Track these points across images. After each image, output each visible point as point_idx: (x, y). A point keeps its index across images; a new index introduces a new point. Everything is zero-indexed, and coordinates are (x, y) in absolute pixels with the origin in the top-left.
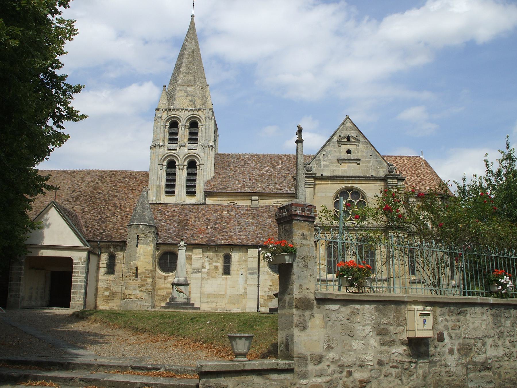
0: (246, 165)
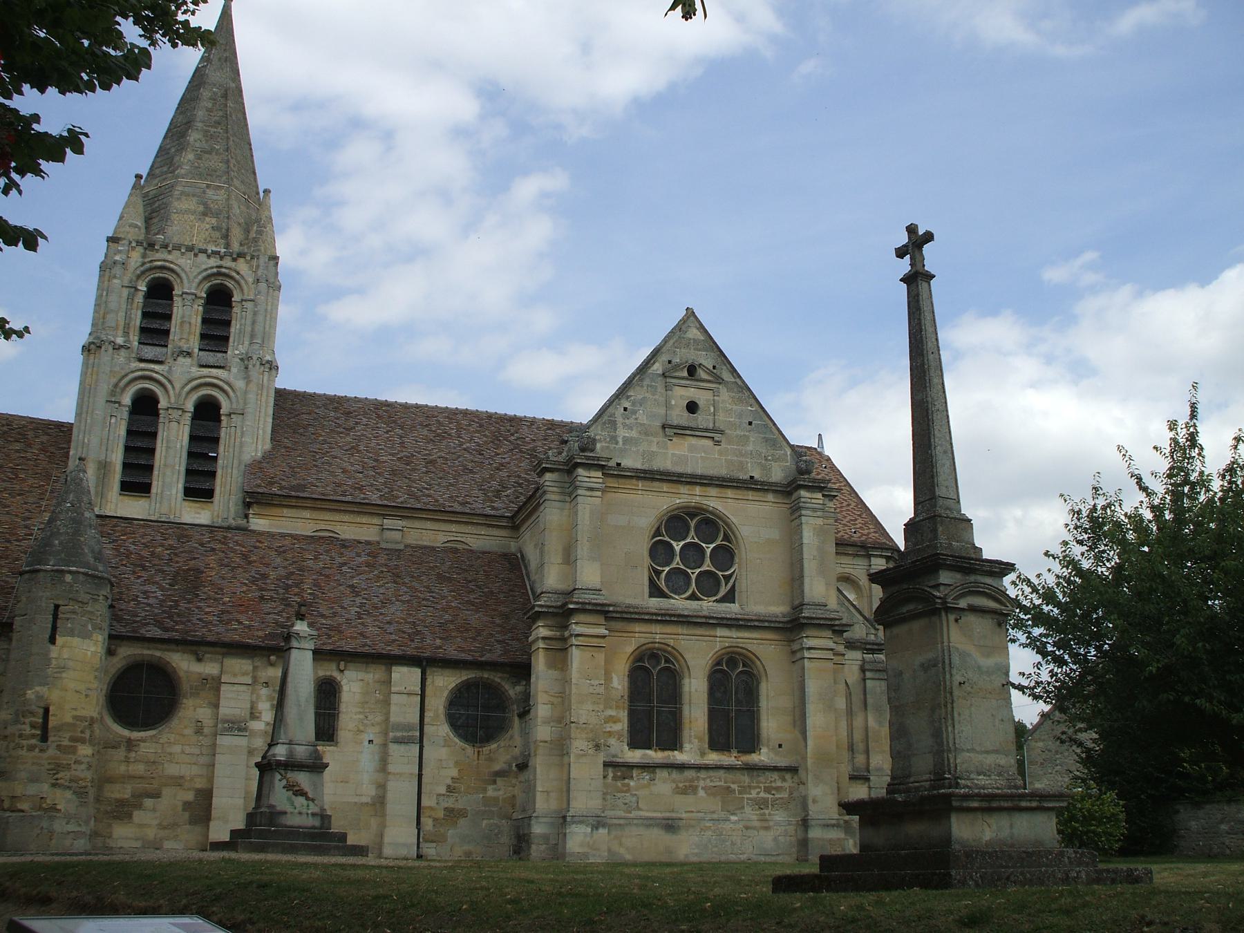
0: (359, 428)
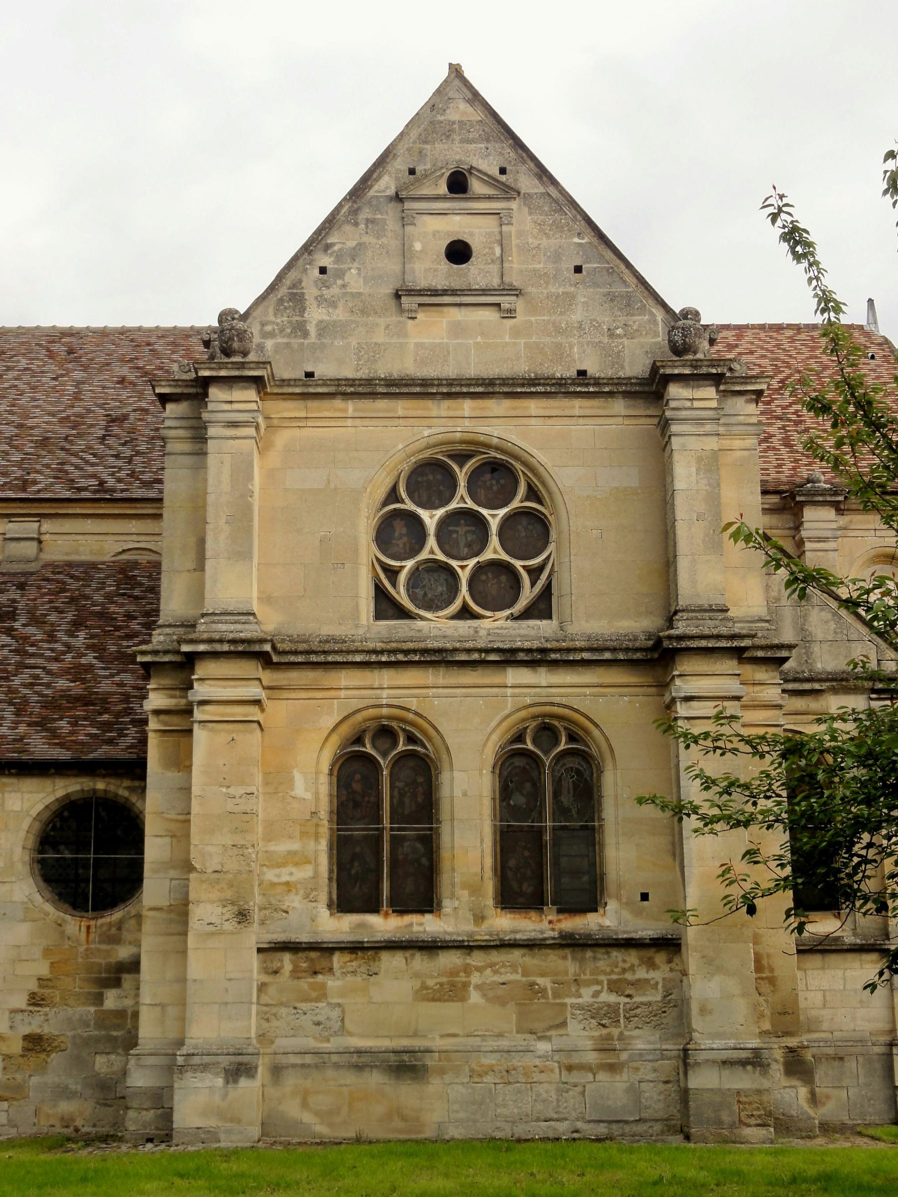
0: (11, 375)
